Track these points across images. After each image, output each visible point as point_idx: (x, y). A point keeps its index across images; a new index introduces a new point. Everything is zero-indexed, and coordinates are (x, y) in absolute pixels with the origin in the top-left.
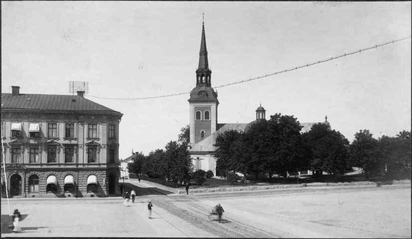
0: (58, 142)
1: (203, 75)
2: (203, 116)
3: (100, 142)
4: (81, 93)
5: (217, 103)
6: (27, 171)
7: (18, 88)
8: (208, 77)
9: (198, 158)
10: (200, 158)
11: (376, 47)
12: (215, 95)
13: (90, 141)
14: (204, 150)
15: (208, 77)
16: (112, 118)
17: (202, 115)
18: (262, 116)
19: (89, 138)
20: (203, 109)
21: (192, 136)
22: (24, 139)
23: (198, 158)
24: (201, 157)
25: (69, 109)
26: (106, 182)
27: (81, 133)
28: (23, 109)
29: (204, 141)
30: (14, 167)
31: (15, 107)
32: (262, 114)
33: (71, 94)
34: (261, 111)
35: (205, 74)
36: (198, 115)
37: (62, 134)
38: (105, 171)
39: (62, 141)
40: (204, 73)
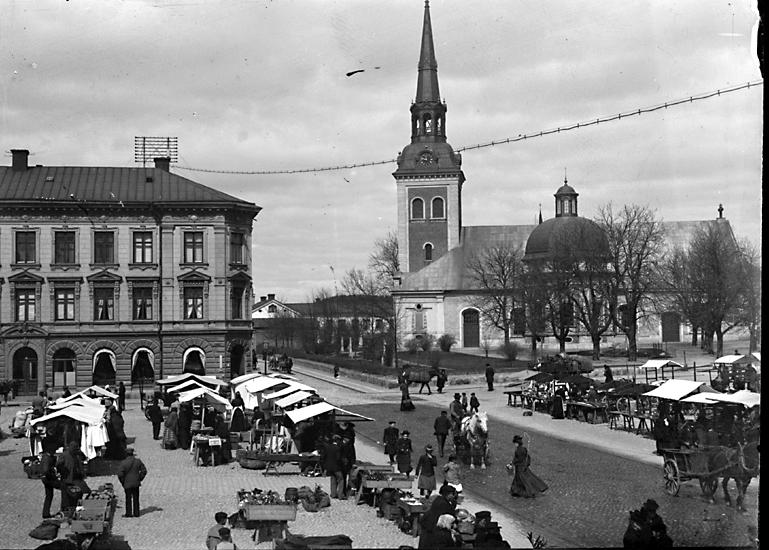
0: (205, 272)
1: (426, 117)
2: (428, 209)
3: (210, 272)
4: (163, 163)
5: (462, 179)
6: (49, 337)
7: (26, 153)
8: (439, 121)
9: (419, 306)
10: (424, 306)
11: (749, 86)
12: (457, 161)
13: (235, 272)
14: (432, 287)
15: (439, 121)
16: (240, 216)
17: (428, 209)
18: (571, 206)
19: (184, 264)
20: (428, 192)
21: (404, 257)
22: (42, 270)
23: (419, 306)
24: (426, 302)
25: (140, 198)
26: (225, 362)
27: (171, 251)
28: (40, 199)
29: (432, 265)
30: (21, 331)
31: (12, 197)
32: (570, 201)
33: (136, 165)
34: (566, 195)
35: (432, 112)
36: (417, 205)
37: (123, 250)
38: (223, 339)
39: (46, 272)
40: (429, 110)
